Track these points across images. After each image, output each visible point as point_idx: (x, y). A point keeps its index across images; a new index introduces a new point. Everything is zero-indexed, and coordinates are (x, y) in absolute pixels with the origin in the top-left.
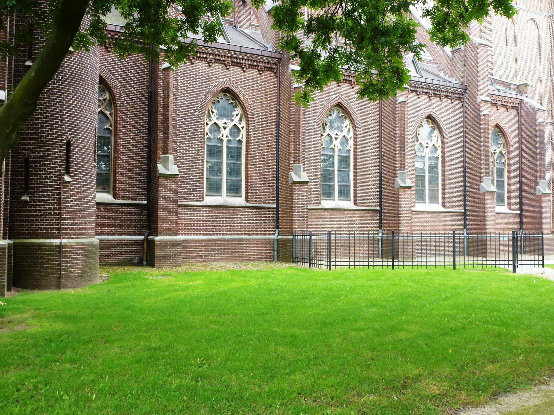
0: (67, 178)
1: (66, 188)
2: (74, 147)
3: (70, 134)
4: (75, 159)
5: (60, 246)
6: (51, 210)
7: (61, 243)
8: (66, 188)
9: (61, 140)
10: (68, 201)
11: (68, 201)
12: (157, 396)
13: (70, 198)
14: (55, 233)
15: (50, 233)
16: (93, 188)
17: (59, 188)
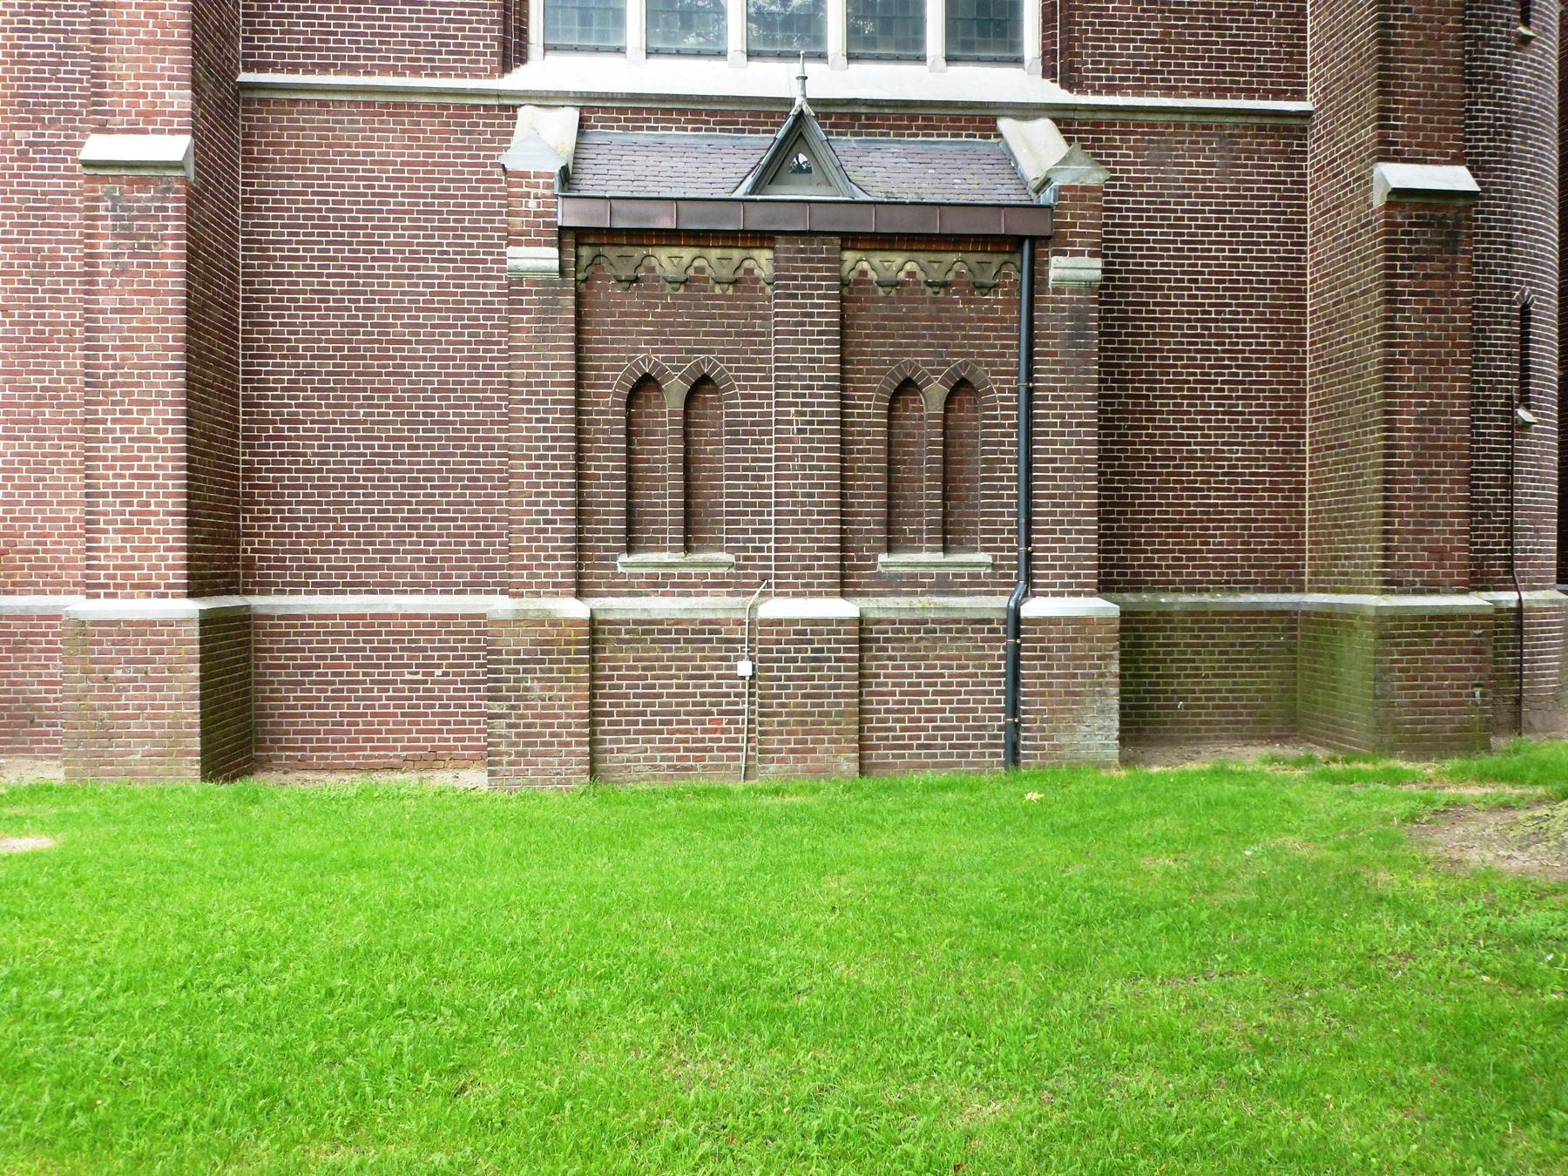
0: (1523, 414)
5: (1519, 610)
6: (1490, 508)
7: (1520, 601)
9: (1509, 302)
12: (1210, 1145)
14: (1498, 573)
15: (1487, 573)
17: (1508, 443)
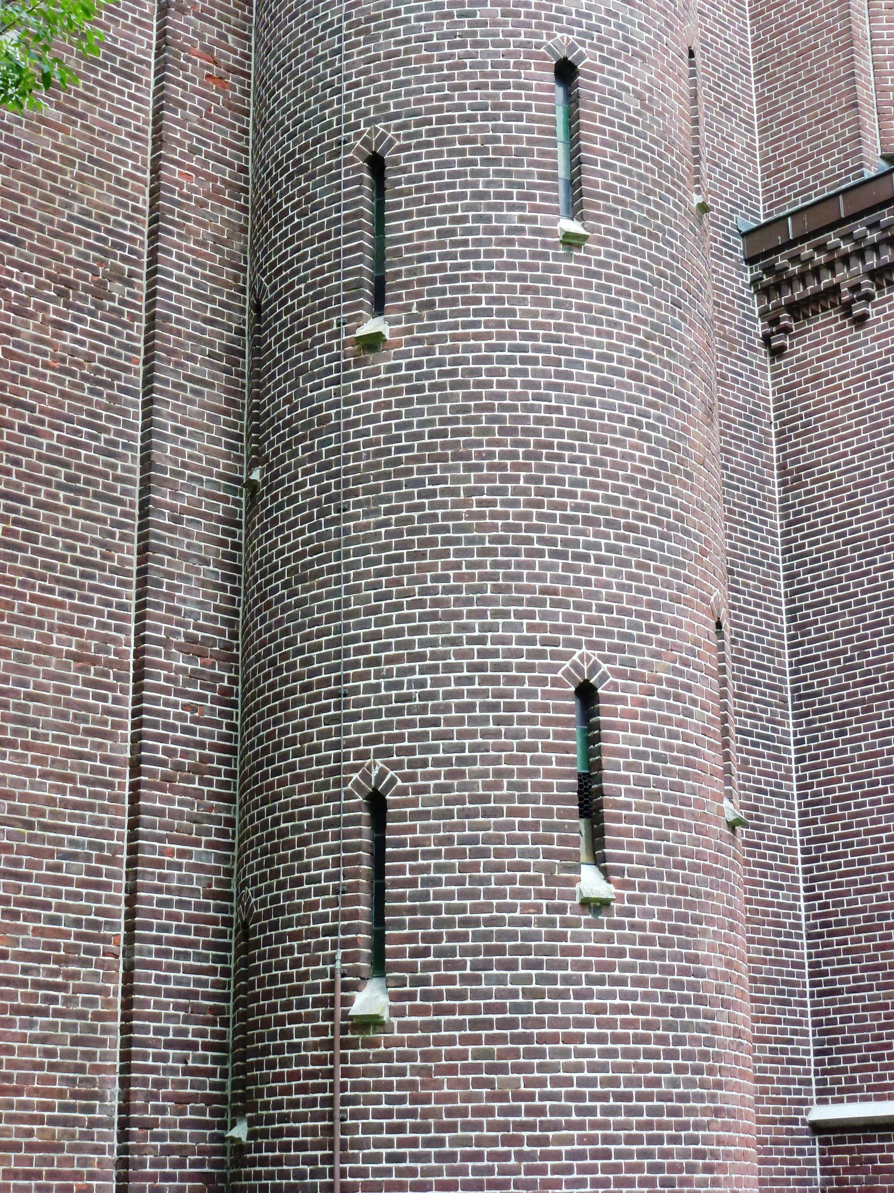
1: (364, 1059)
2: (402, 817)
3: (379, 753)
4: (412, 883)
8: (364, 1059)
10: (378, 1129)
11: (378, 1129)
13: (388, 1114)
16: (737, 1087)
